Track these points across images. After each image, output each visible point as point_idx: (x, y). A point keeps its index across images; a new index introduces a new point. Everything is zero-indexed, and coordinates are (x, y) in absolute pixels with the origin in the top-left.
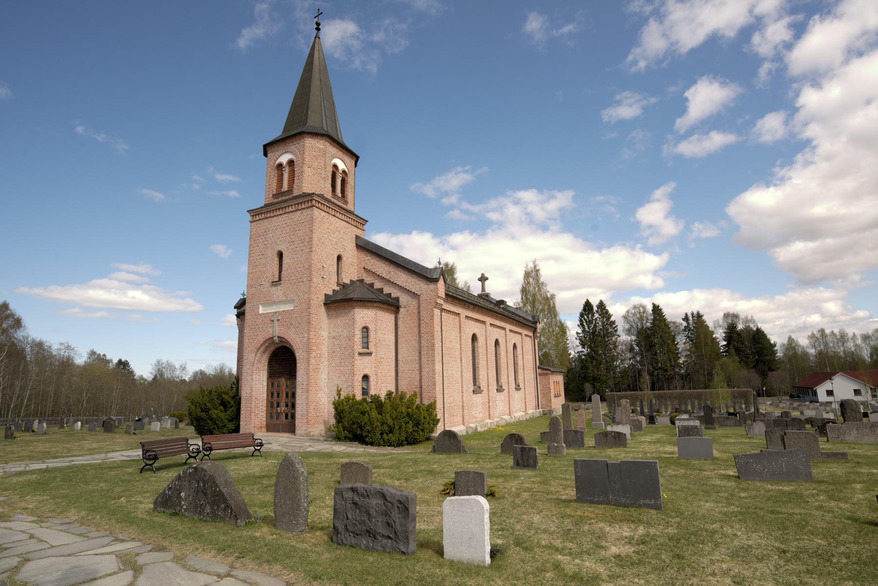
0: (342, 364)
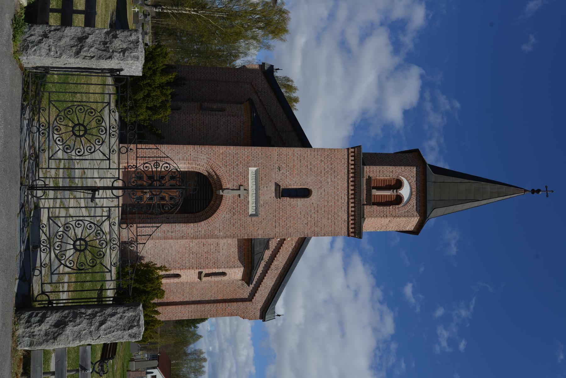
0: (191, 255)
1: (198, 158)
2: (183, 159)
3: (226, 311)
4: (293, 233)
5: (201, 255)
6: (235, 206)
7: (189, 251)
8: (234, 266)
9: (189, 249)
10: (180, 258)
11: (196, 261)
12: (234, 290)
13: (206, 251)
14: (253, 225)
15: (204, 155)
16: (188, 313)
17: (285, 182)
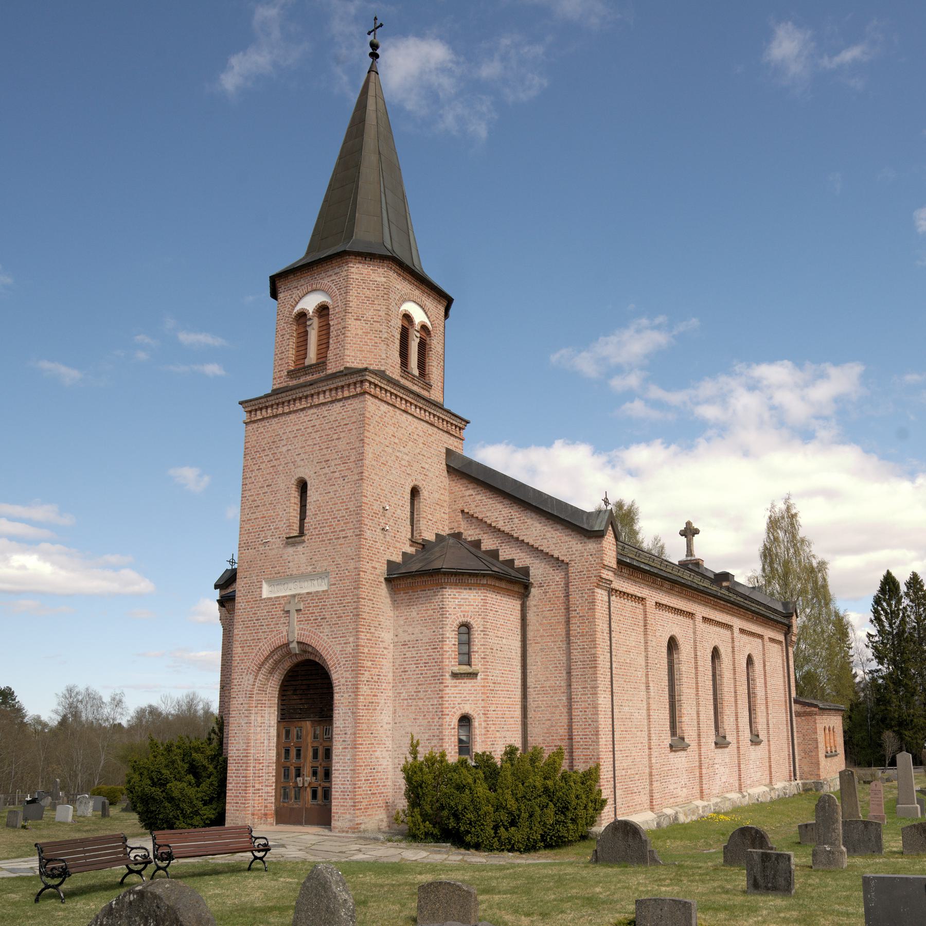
0: (421, 695)
1: (246, 690)
2: (247, 717)
3: (585, 616)
4: (356, 502)
5: (421, 676)
6: (312, 618)
7: (415, 699)
8: (441, 608)
9: (410, 699)
10: (424, 716)
11: (430, 684)
12: (550, 601)
13: (415, 666)
14: (341, 580)
15: (243, 680)
16: (587, 694)
17: (284, 530)
